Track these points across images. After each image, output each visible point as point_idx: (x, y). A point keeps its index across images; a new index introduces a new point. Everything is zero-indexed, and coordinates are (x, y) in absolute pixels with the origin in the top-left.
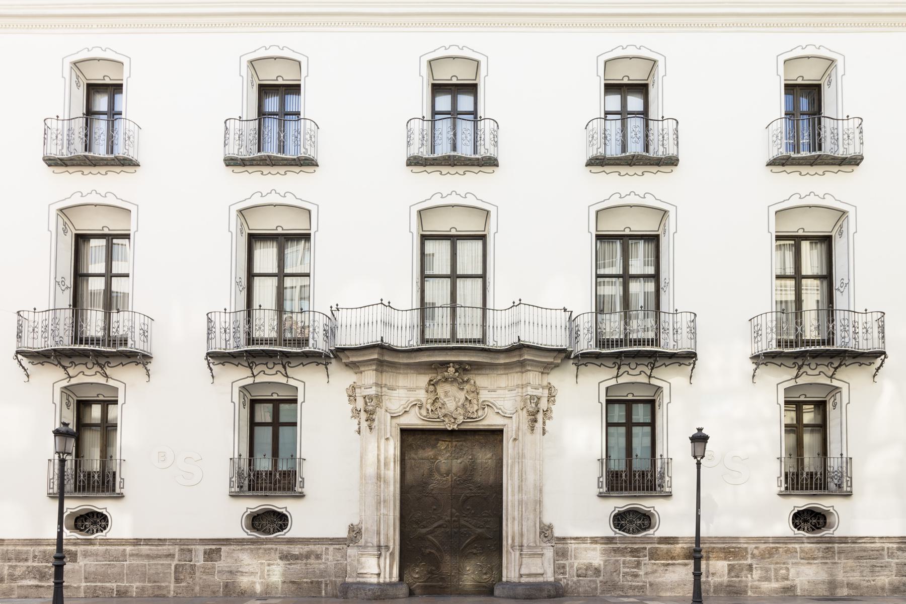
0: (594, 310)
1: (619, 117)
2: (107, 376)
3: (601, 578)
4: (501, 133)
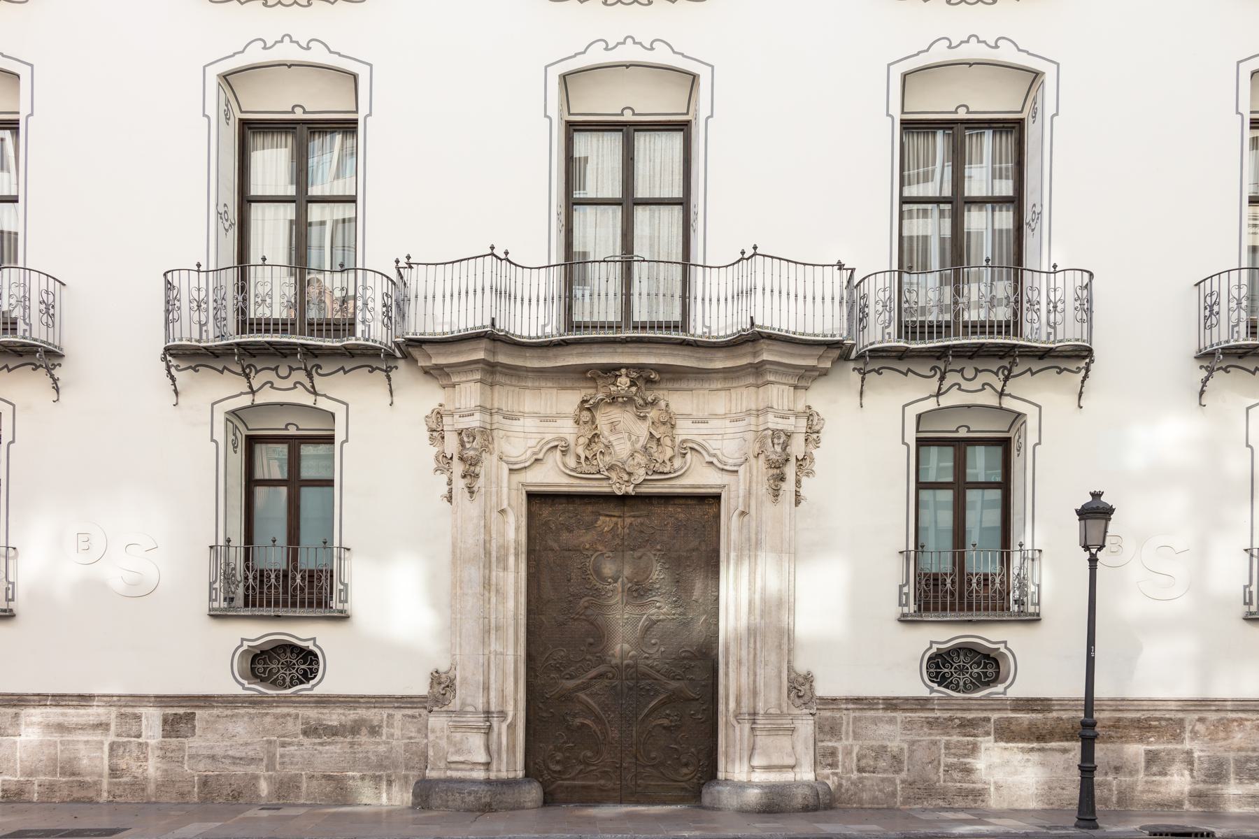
0: (895, 267)
2: (315, 393)
3: (904, 775)
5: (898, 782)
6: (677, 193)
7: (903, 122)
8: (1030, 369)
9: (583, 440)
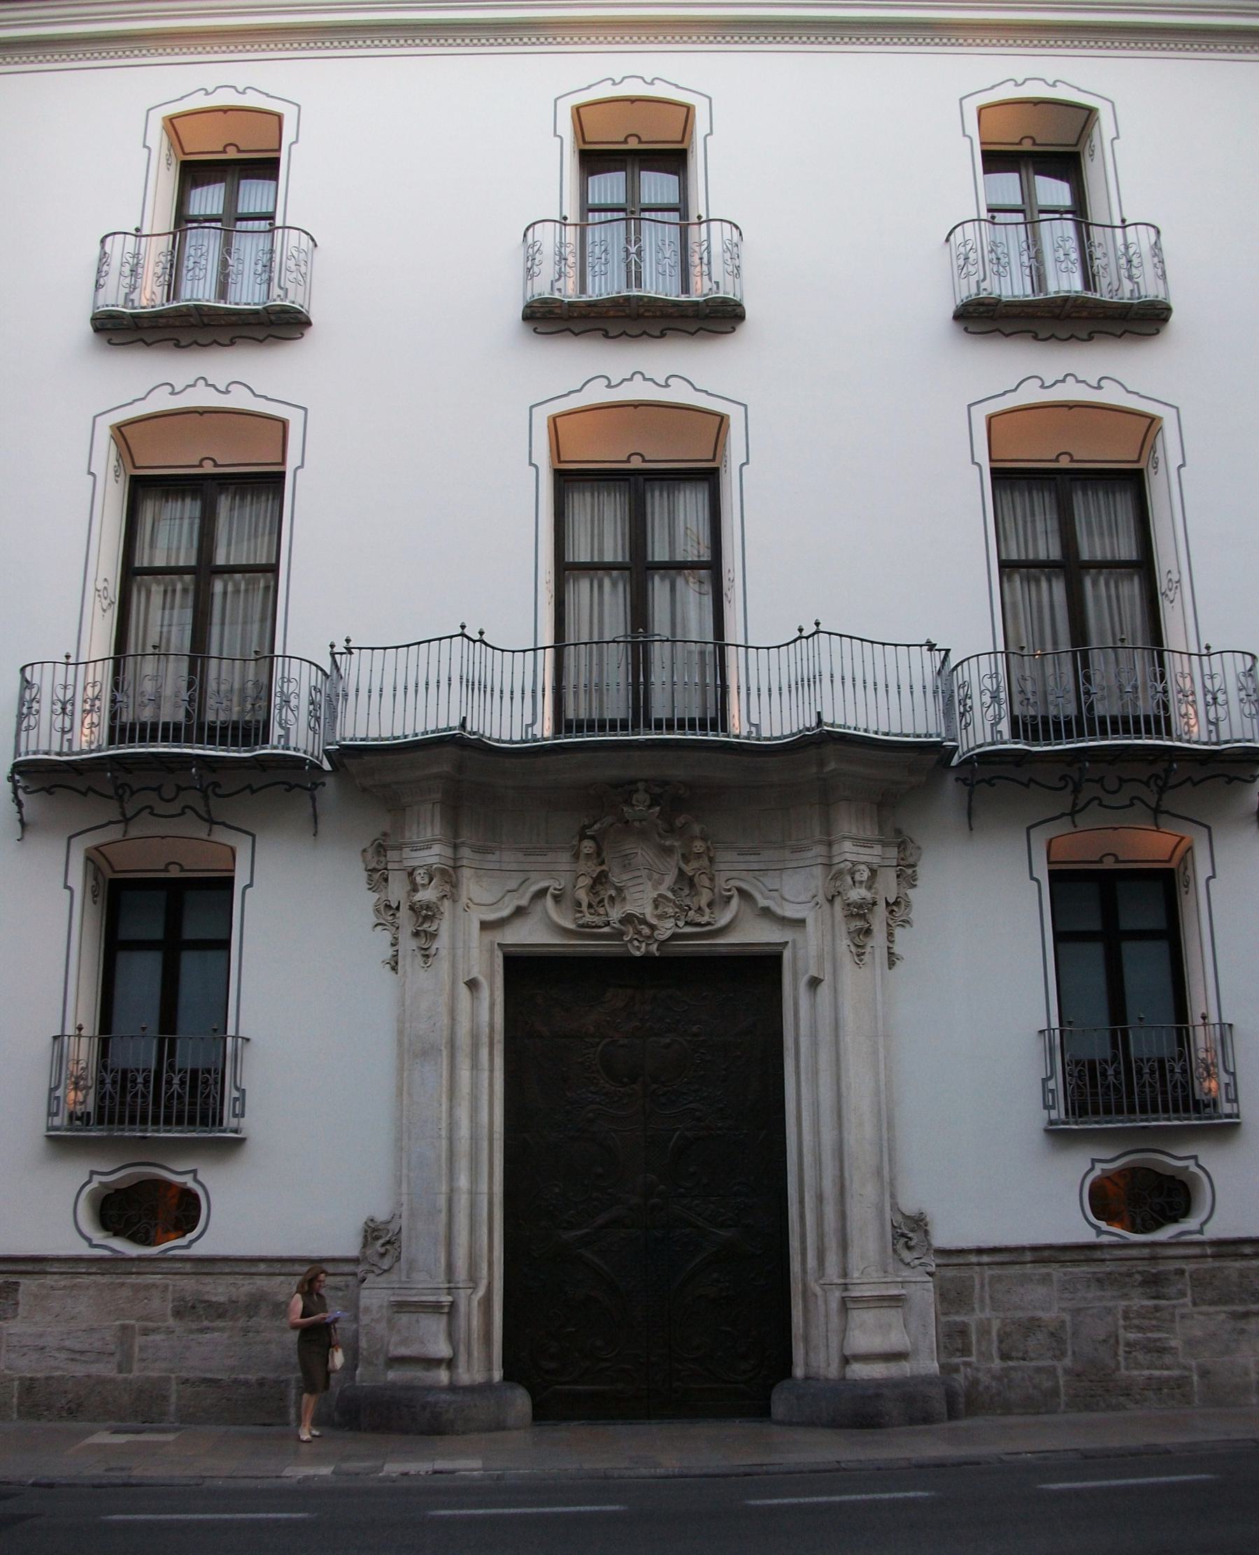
0: (1001, 647)
1: (1019, 217)
3: (1068, 1361)
4: (744, 250)
5: (1060, 1372)
6: (706, 556)
7: (993, 471)
8: (249, 786)
9: (585, 881)
